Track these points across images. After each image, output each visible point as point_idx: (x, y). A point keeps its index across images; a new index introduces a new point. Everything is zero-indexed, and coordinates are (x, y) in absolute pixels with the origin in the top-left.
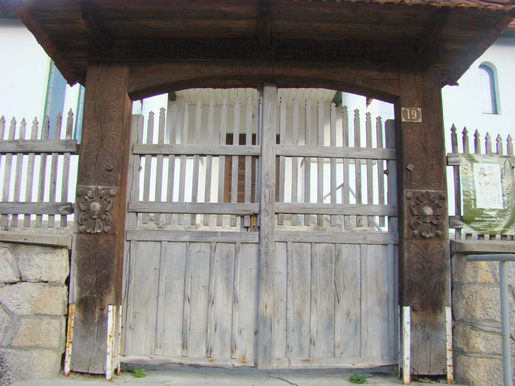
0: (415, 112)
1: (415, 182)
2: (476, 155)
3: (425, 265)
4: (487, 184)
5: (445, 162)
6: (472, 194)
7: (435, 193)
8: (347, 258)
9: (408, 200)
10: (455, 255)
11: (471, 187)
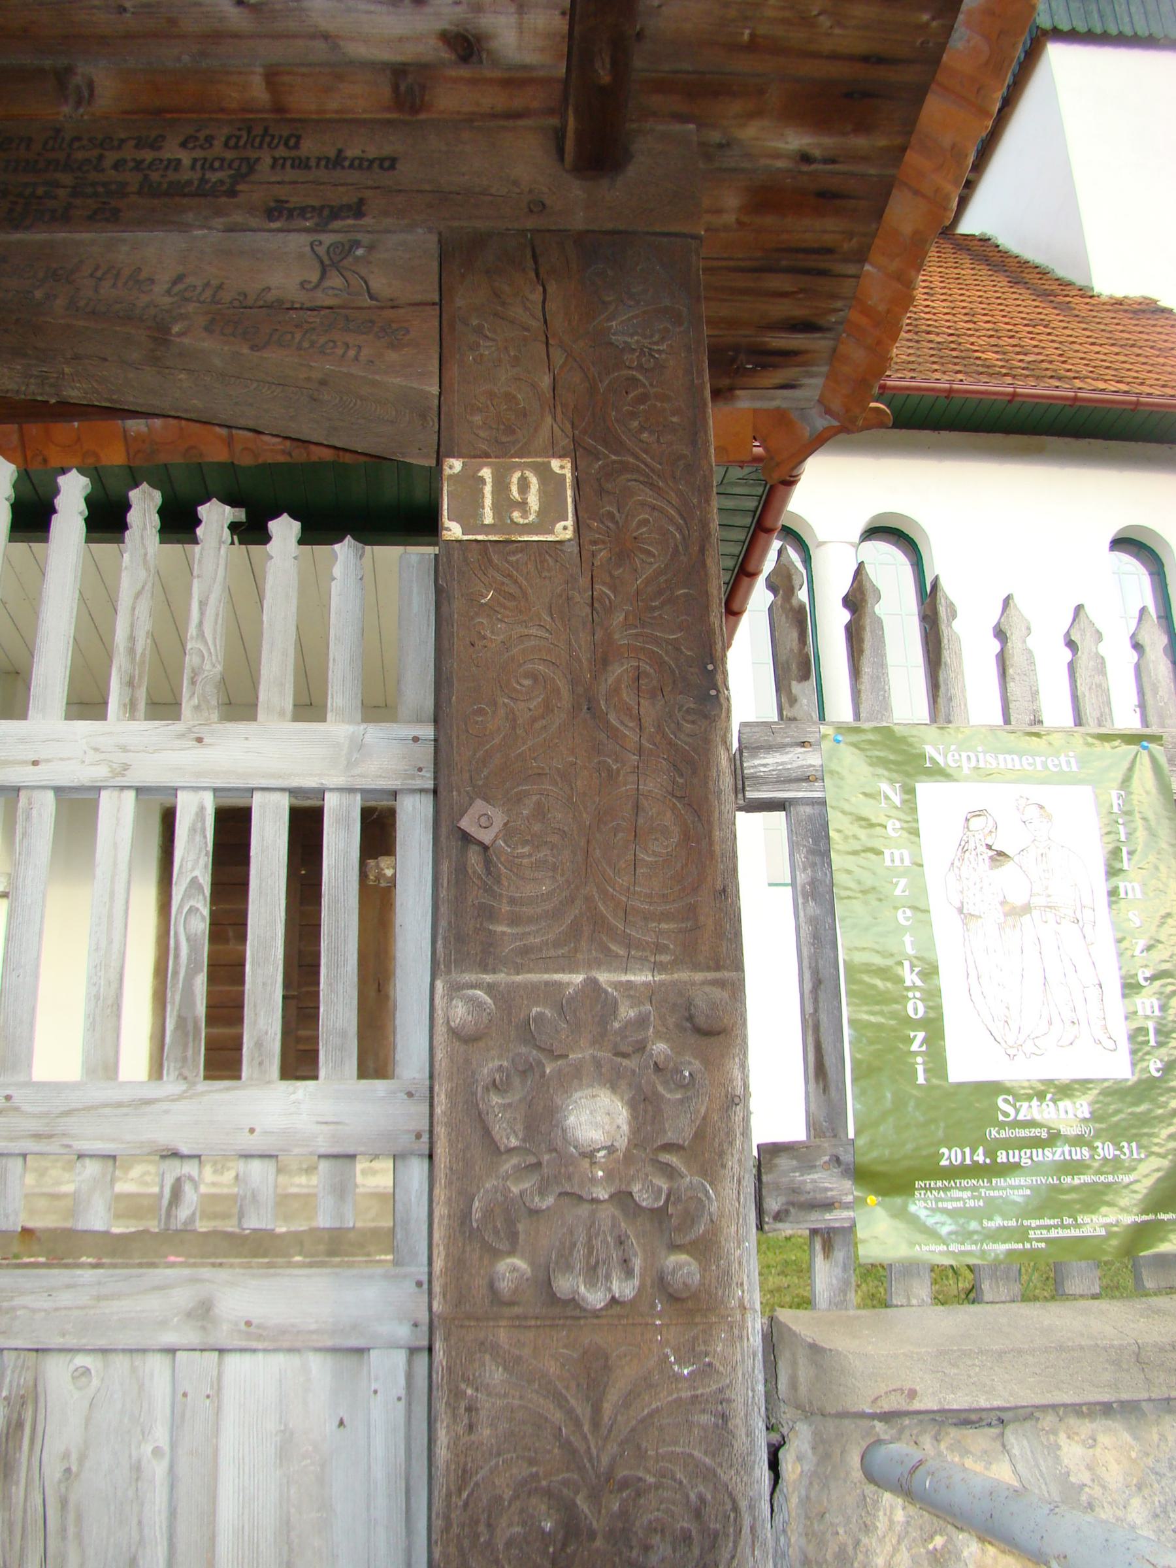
0: (534, 481)
1: (514, 920)
2: (932, 732)
3: (581, 1502)
4: (1017, 912)
5: (727, 782)
6: (914, 987)
7: (651, 993)
8: (74, 1456)
11: (907, 939)
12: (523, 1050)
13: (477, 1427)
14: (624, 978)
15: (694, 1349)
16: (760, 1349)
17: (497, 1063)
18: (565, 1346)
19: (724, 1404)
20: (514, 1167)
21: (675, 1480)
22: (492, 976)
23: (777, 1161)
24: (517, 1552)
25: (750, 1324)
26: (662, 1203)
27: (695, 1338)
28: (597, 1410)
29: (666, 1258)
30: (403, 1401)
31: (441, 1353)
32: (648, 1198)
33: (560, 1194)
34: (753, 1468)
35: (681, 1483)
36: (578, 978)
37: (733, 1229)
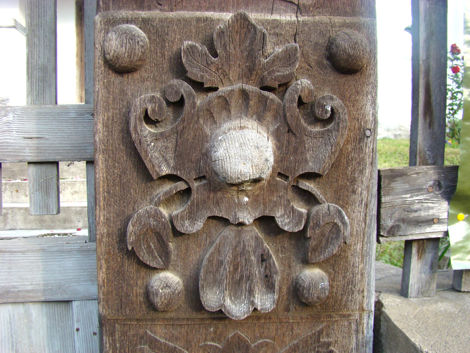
9: (113, 77)
12: (176, 82)
14: (270, 17)
15: (319, 341)
16: (372, 339)
17: (150, 94)
18: (213, 340)
20: (166, 193)
22: (147, 12)
23: (394, 185)
25: (365, 321)
26: (301, 228)
29: (301, 272)
31: (108, 345)
32: (289, 223)
33: (209, 218)
36: (228, 16)
37: (359, 246)
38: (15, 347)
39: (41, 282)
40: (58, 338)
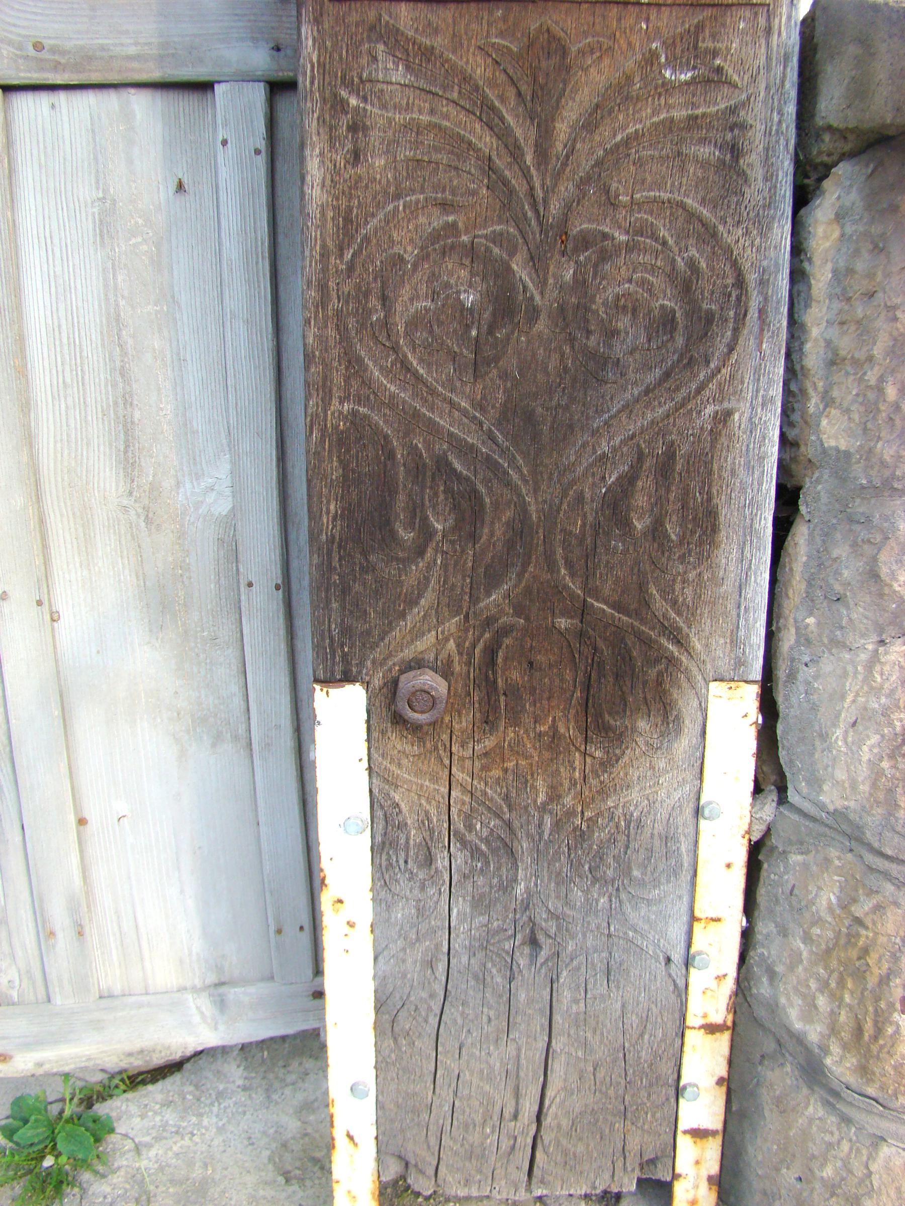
3: (520, 269)
10: (843, 170)
13: (365, 155)
15: (696, 47)
16: (797, 49)
18: (501, 34)
19: (736, 131)
21: (656, 240)
24: (425, 335)
27: (700, 28)
28: (545, 133)
30: (264, 154)
31: (310, 42)
34: (770, 228)
35: (665, 243)
38: (101, 182)
39: (153, 40)
40: (185, 165)
